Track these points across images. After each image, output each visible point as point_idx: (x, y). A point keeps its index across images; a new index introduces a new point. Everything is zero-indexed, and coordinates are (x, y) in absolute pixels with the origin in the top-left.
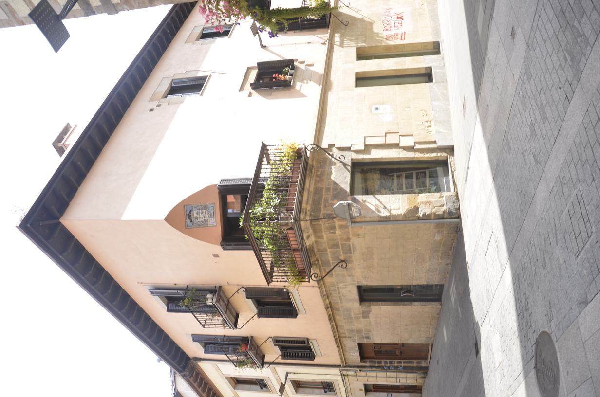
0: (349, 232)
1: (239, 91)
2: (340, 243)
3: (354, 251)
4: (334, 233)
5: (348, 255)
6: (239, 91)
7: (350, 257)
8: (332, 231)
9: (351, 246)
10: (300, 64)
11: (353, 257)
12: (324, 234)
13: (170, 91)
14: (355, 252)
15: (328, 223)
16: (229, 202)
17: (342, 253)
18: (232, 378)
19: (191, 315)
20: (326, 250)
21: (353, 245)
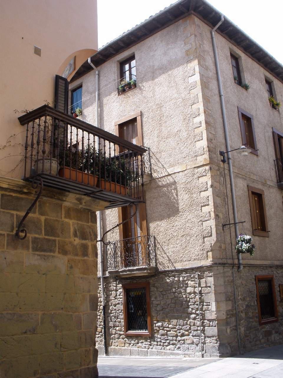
0: (77, 255)
1: (40, 56)
2: (57, 239)
3: (39, 255)
4: (75, 235)
5: (31, 245)
6: (40, 56)
7: (27, 248)
8: (78, 233)
9: (52, 254)
10: (76, 70)
11: (25, 252)
12: (73, 221)
13: (244, 114)
14: (36, 257)
15: (90, 233)
16: (98, 366)
17: (37, 236)
18: (82, 85)
19: (132, 69)
20: (42, 214)
21: (53, 257)
